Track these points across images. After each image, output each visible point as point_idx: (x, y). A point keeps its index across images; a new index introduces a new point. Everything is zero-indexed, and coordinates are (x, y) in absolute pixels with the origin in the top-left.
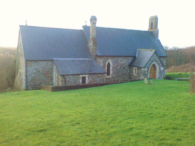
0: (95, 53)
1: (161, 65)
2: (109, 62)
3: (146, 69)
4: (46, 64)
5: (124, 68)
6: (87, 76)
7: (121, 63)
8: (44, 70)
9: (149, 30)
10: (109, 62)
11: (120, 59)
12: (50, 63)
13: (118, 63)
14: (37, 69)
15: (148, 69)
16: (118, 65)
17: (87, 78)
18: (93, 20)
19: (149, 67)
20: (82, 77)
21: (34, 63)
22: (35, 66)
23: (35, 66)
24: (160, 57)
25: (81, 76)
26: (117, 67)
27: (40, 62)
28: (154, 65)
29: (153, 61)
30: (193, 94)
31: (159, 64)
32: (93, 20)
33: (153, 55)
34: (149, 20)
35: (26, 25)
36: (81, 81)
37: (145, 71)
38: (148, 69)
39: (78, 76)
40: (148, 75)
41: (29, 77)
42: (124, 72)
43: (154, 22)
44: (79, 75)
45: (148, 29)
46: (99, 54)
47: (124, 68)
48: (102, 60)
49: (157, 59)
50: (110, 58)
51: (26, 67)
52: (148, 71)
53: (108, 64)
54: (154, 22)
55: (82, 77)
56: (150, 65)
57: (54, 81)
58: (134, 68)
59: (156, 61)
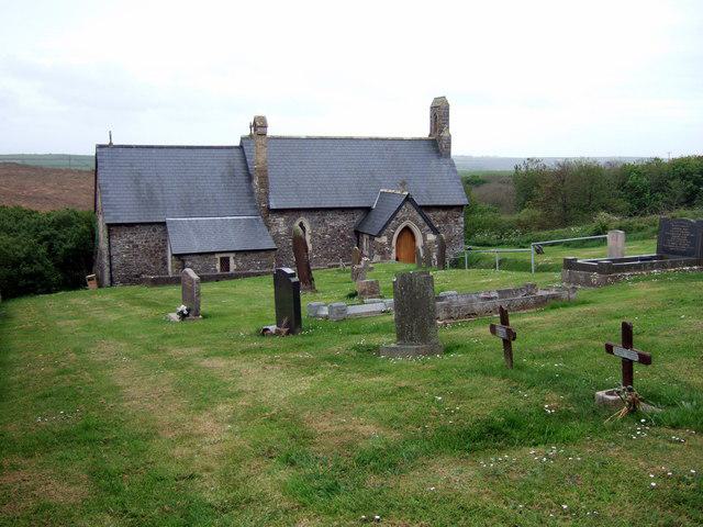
1: (427, 227)
3: (384, 239)
5: (343, 236)
6: (232, 256)
9: (430, 135)
12: (358, 217)
15: (390, 239)
17: (232, 261)
20: (221, 259)
25: (218, 256)
28: (407, 229)
29: (404, 219)
32: (259, 125)
33: (400, 207)
35: (111, 143)
36: (218, 266)
37: (382, 244)
38: (390, 239)
39: (212, 257)
40: (390, 252)
43: (440, 114)
44: (213, 253)
45: (428, 132)
47: (343, 236)
51: (109, 237)
52: (390, 244)
54: (440, 114)
55: (221, 259)
56: (396, 229)
57: (170, 270)
58: (365, 236)
59: (412, 219)
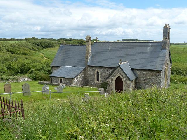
2: (98, 71)
7: (107, 72)
10: (98, 71)
11: (107, 69)
16: (106, 74)
18: (167, 30)
31: (124, 78)
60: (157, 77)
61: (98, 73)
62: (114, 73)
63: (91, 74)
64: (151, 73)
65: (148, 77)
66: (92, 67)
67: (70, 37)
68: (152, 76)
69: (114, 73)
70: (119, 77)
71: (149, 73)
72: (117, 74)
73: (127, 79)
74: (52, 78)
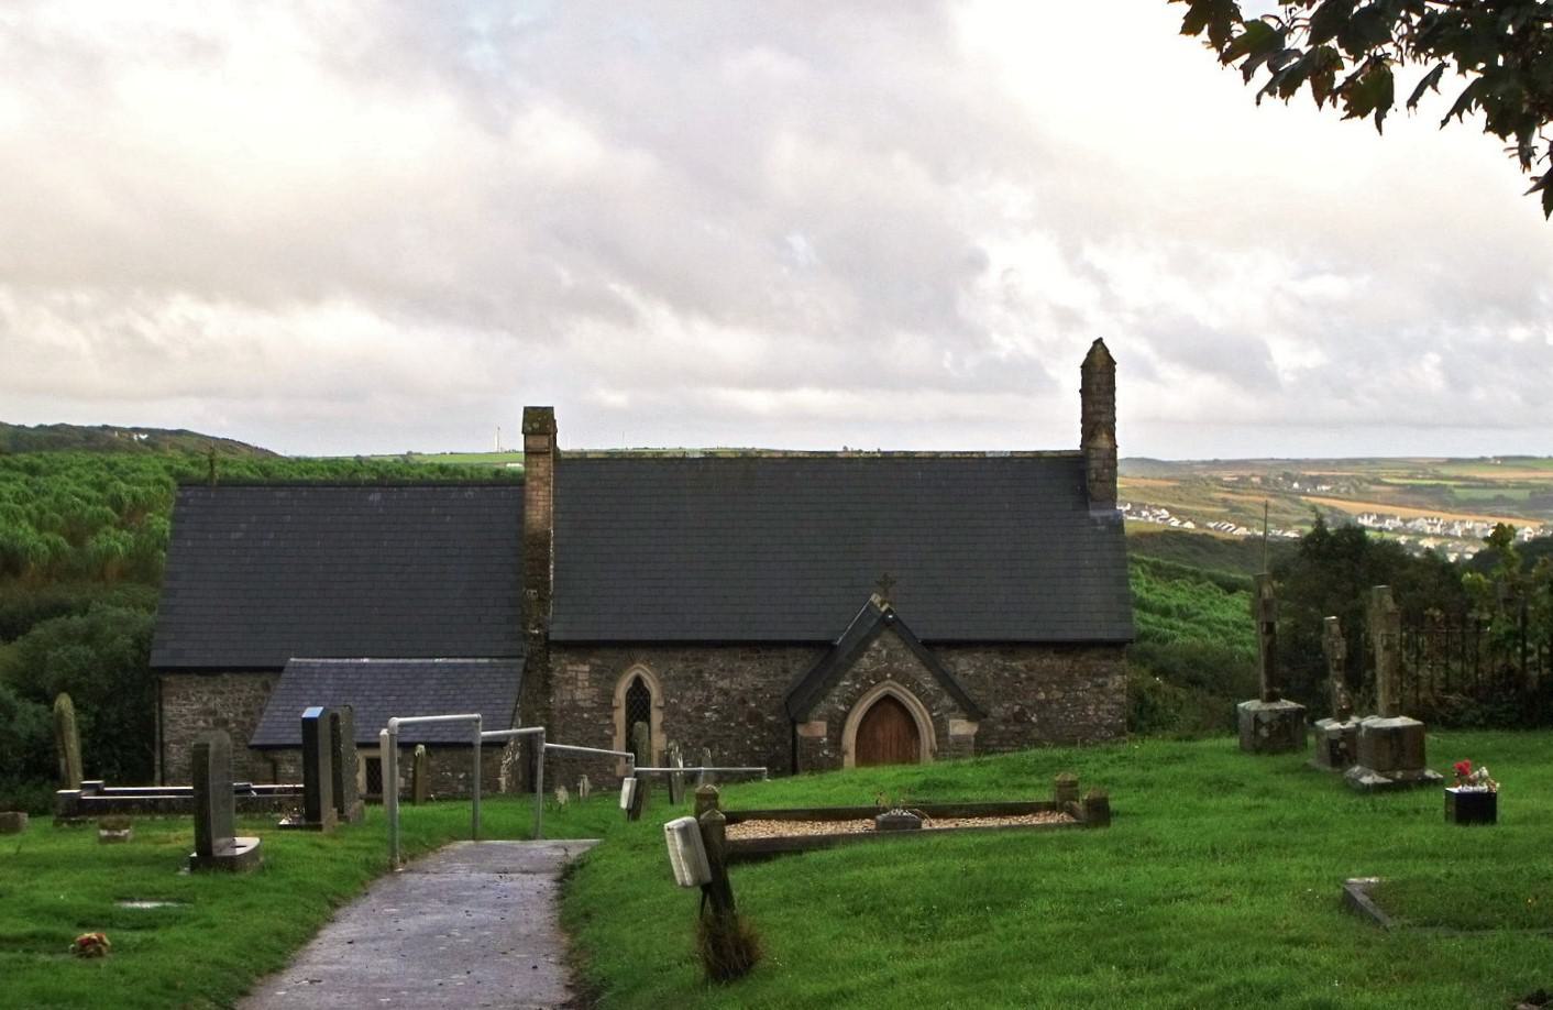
0: (539, 626)
1: (947, 701)
2: (638, 681)
4: (257, 686)
7: (725, 684)
8: (247, 720)
10: (638, 681)
11: (718, 660)
13: (706, 686)
14: (213, 713)
16: (708, 699)
18: (539, 423)
19: (846, 715)
21: (197, 682)
22: (205, 699)
23: (205, 699)
24: (930, 645)
26: (701, 709)
27: (226, 676)
30: (1551, 941)
31: (928, 703)
34: (358, 457)
41: (174, 751)
42: (755, 743)
46: (557, 633)
48: (587, 668)
49: (911, 664)
50: (643, 655)
53: (630, 693)
59: (903, 678)
60: (1101, 686)
61: (638, 694)
62: (856, 677)
63: (574, 706)
64: (1062, 664)
65: (1042, 696)
66: (581, 648)
67: (1363, 476)
68: (1067, 682)
69: (856, 677)
70: (888, 700)
71: (1046, 662)
72: (879, 678)
73: (953, 709)
74: (278, 756)
